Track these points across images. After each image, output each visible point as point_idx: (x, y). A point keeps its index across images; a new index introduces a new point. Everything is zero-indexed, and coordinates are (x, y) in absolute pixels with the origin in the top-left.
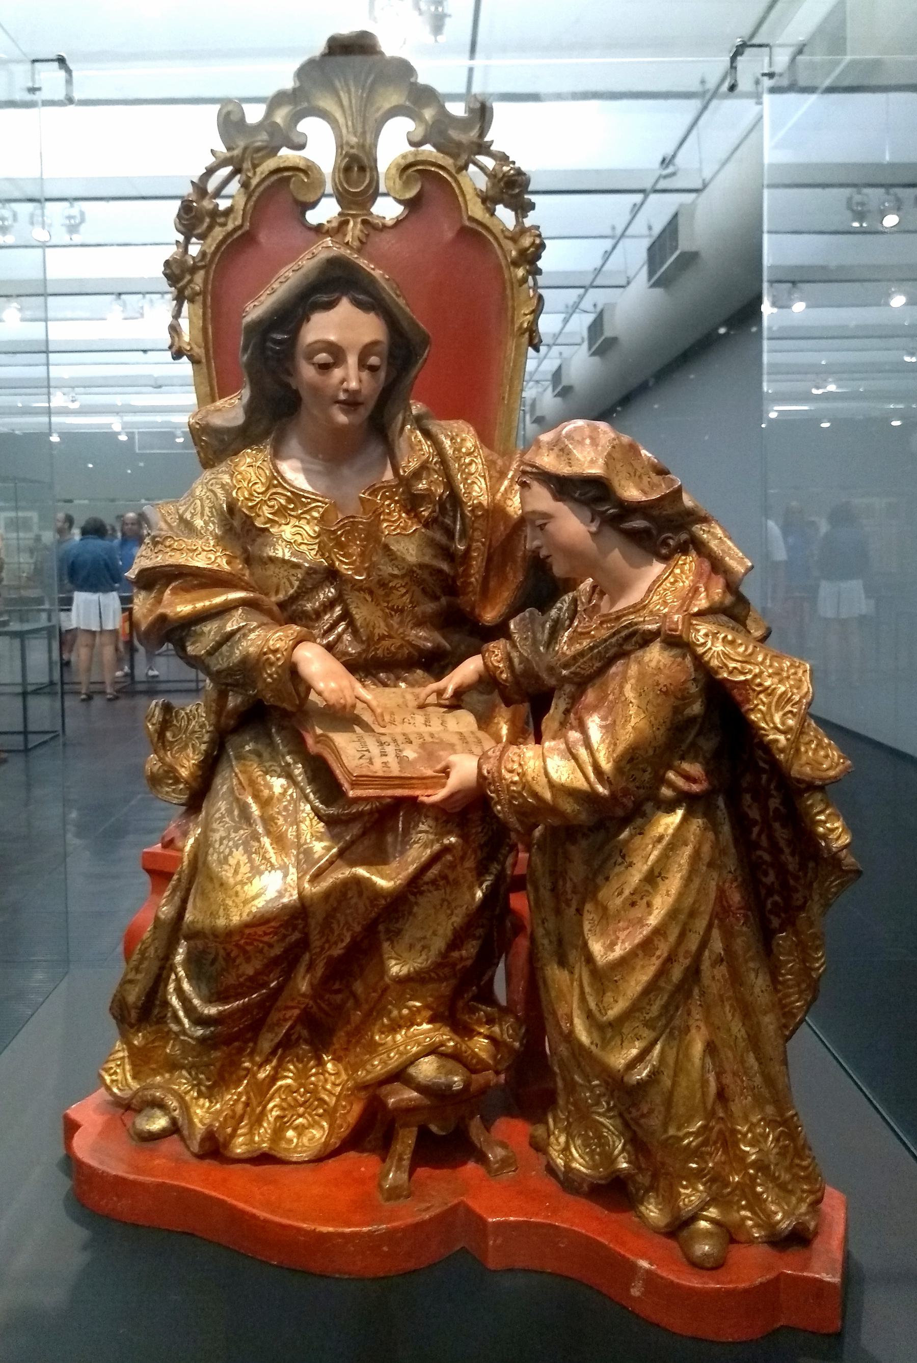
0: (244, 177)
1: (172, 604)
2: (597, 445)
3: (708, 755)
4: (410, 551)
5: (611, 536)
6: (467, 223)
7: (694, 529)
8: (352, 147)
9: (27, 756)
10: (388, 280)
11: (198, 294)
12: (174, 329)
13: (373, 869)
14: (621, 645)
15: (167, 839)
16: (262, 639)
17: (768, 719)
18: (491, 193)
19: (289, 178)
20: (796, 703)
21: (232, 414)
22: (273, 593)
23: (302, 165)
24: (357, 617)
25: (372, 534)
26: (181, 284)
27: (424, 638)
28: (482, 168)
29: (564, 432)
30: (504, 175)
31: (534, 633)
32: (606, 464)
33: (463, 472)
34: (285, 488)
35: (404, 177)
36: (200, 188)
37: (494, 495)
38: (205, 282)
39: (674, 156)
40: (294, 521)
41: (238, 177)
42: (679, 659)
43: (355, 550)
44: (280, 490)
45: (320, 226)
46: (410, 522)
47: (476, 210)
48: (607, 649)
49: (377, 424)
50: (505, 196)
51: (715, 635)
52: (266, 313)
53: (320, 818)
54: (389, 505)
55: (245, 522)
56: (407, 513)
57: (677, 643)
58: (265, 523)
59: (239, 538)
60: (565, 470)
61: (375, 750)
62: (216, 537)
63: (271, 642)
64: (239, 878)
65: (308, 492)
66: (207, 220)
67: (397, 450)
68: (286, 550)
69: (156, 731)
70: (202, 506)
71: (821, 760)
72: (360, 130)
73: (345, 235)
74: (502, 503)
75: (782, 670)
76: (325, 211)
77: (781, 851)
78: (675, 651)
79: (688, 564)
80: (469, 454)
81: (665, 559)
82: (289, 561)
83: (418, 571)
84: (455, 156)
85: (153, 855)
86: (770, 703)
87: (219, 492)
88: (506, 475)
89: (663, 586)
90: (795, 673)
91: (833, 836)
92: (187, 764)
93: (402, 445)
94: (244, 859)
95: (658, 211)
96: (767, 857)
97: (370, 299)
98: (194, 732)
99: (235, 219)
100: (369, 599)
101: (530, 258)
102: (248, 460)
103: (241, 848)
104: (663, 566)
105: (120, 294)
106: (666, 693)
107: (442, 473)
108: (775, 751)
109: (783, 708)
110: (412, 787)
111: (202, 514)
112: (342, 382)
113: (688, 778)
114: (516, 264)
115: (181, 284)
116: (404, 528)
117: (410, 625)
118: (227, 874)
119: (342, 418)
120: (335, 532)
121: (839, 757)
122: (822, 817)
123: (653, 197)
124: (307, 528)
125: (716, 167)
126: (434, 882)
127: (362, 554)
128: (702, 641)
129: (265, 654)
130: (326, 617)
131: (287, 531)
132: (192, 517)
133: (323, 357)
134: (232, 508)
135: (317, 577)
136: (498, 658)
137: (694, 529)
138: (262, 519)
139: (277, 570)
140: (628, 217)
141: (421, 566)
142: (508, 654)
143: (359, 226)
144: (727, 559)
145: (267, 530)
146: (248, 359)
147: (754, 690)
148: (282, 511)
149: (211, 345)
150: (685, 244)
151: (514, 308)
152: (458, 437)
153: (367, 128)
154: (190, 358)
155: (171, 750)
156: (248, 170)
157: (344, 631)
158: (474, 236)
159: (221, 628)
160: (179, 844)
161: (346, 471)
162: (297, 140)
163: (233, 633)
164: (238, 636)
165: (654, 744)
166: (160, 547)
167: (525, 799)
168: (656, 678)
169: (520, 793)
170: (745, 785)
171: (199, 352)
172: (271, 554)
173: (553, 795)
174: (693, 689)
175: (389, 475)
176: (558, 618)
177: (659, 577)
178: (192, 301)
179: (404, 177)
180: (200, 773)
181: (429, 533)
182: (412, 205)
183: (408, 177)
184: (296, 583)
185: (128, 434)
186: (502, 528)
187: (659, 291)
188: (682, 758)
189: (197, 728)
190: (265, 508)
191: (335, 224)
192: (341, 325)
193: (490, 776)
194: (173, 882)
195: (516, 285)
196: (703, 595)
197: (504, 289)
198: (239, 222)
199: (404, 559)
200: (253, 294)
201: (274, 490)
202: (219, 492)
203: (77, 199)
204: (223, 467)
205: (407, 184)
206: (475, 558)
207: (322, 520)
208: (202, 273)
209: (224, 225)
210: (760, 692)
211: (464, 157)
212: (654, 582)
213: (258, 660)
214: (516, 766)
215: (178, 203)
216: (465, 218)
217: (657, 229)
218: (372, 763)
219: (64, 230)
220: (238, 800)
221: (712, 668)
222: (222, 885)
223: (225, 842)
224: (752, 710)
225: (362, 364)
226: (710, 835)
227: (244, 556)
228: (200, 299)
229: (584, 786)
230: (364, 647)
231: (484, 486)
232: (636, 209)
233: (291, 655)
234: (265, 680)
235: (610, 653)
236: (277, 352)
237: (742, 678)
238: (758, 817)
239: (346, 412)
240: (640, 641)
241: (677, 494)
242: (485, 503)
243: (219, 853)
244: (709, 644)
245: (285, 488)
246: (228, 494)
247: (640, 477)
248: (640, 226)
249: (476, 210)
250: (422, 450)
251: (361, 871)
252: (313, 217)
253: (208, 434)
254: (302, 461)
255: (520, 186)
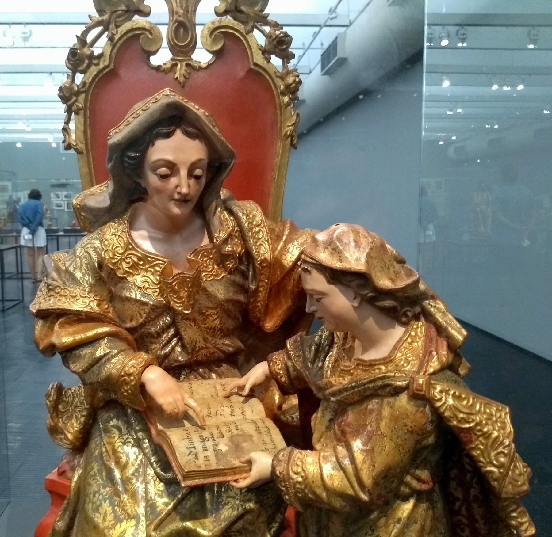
0: (110, 34)
1: (59, 336)
2: (360, 247)
3: (433, 464)
4: (220, 291)
5: (368, 309)
6: (253, 67)
7: (424, 303)
8: (180, 16)
9: (4, 313)
10: (207, 116)
11: (81, 109)
12: (65, 130)
13: (197, 522)
14: (376, 390)
15: (61, 470)
16: (121, 362)
17: (486, 455)
18: (267, 48)
19: (139, 35)
20: (507, 446)
21: (101, 198)
22: (128, 321)
23: (147, 26)
24: (185, 337)
25: (196, 282)
26: (70, 103)
27: (229, 344)
28: (262, 32)
29: (335, 235)
30: (276, 37)
31: (304, 353)
32: (367, 262)
33: (254, 238)
34: (137, 251)
35: (213, 36)
36: (82, 40)
37: (273, 252)
38: (86, 101)
39: (336, 7)
40: (143, 273)
41: (106, 33)
42: (422, 409)
43: (183, 294)
44: (134, 252)
45: (159, 66)
46: (220, 272)
47: (259, 58)
48: (365, 390)
49: (200, 208)
50: (277, 50)
51: (447, 392)
52: (123, 138)
53: (161, 480)
54: (206, 261)
55: (110, 273)
56: (218, 265)
57: (420, 398)
58: (124, 274)
59: (106, 284)
60: (337, 265)
61: (199, 446)
62: (91, 285)
63: (127, 369)
64: (106, 524)
65: (153, 254)
66: (87, 61)
67: (212, 226)
68: (138, 293)
69: (52, 406)
70: (81, 263)
71: (517, 478)
72: (184, 5)
73: (175, 73)
74: (279, 257)
75: (492, 415)
76: (162, 57)
77: (476, 521)
78: (420, 402)
79: (420, 328)
80: (258, 225)
81: (405, 324)
82: (140, 301)
83: (226, 305)
84: (244, 23)
85: (52, 481)
86: (487, 444)
87: (93, 254)
88: (282, 238)
89: (404, 345)
90: (500, 417)
91: (523, 528)
92: (73, 427)
93: (216, 222)
94: (109, 510)
95: (327, 36)
96: (465, 521)
97: (197, 131)
98: (76, 407)
99: (104, 61)
100: (193, 325)
101: (292, 90)
102: (113, 230)
103: (107, 501)
104: (403, 329)
105: (51, 73)
106: (412, 432)
107: (240, 238)
108: (490, 479)
109: (497, 448)
110: (225, 475)
111: (81, 269)
112: (177, 186)
113: (419, 480)
114: (283, 94)
115: (70, 103)
116: (216, 276)
117: (219, 337)
118: (98, 519)
119: (176, 210)
120: (171, 284)
121: (524, 467)
122: (515, 514)
123: (325, 29)
124: (152, 277)
125: (357, 14)
126: (239, 532)
127: (189, 296)
128: (438, 397)
129: (123, 376)
130: (164, 336)
131: (139, 279)
132: (74, 271)
133: (163, 170)
134: (101, 265)
135: (159, 311)
136: (279, 367)
137: (424, 303)
138: (121, 270)
139: (131, 306)
140: (311, 39)
141: (228, 301)
142: (286, 364)
143: (184, 68)
144: (450, 329)
145: (125, 278)
146: (112, 166)
147: (476, 434)
148: (135, 266)
149: (89, 141)
150: (340, 54)
151: (281, 122)
152: (251, 212)
153: (189, 4)
154: (76, 150)
155: (62, 418)
156: (113, 29)
157: (176, 345)
158: (257, 75)
159: (93, 354)
160: (69, 474)
161: (178, 238)
162: (146, 10)
163: (101, 358)
164: (104, 360)
165: (401, 465)
166: (52, 293)
167: (306, 495)
168: (405, 421)
169: (303, 490)
170: (452, 476)
171: (82, 146)
172: (127, 295)
173: (327, 496)
174: (430, 427)
175: (206, 241)
176: (320, 343)
177: (401, 339)
178: (77, 113)
179: (213, 36)
180: (81, 436)
181: (232, 277)
182: (218, 54)
183: (215, 36)
184: (144, 316)
185: (56, 143)
186: (279, 273)
187: (326, 77)
188: (417, 468)
189: (79, 404)
190: (124, 264)
191: (169, 66)
192: (177, 149)
193: (281, 476)
194: (64, 505)
195: (283, 108)
196: (435, 357)
197: (276, 109)
198: (106, 63)
199: (216, 297)
200: (115, 124)
201: (130, 252)
202: (93, 254)
203: (27, 24)
204: (95, 235)
205: (215, 41)
206: (260, 292)
207: (163, 274)
208: (83, 96)
209: (97, 65)
210: (479, 436)
211: (251, 24)
212: (398, 342)
213: (118, 381)
214: (300, 470)
215: (69, 49)
216: (251, 63)
217: (326, 45)
218: (197, 459)
219: (21, 40)
220: (105, 465)
221: (446, 417)
222: (95, 528)
223: (97, 495)
224: (474, 448)
225: (190, 174)
226: (430, 512)
227: (110, 295)
228: (82, 112)
229: (350, 492)
230: (190, 357)
231: (267, 247)
232: (316, 35)
233: (140, 378)
234: (123, 393)
235: (368, 393)
236: (133, 164)
237: (468, 426)
238: (461, 496)
239: (179, 207)
240: (392, 391)
241: (416, 283)
242: (269, 258)
243: (93, 503)
244: (444, 399)
245: (137, 251)
246: (99, 255)
247: (388, 268)
248: (317, 44)
249: (259, 58)
250: (228, 224)
251: (189, 524)
252: (155, 60)
253: (85, 212)
254: (148, 232)
255: (286, 44)
